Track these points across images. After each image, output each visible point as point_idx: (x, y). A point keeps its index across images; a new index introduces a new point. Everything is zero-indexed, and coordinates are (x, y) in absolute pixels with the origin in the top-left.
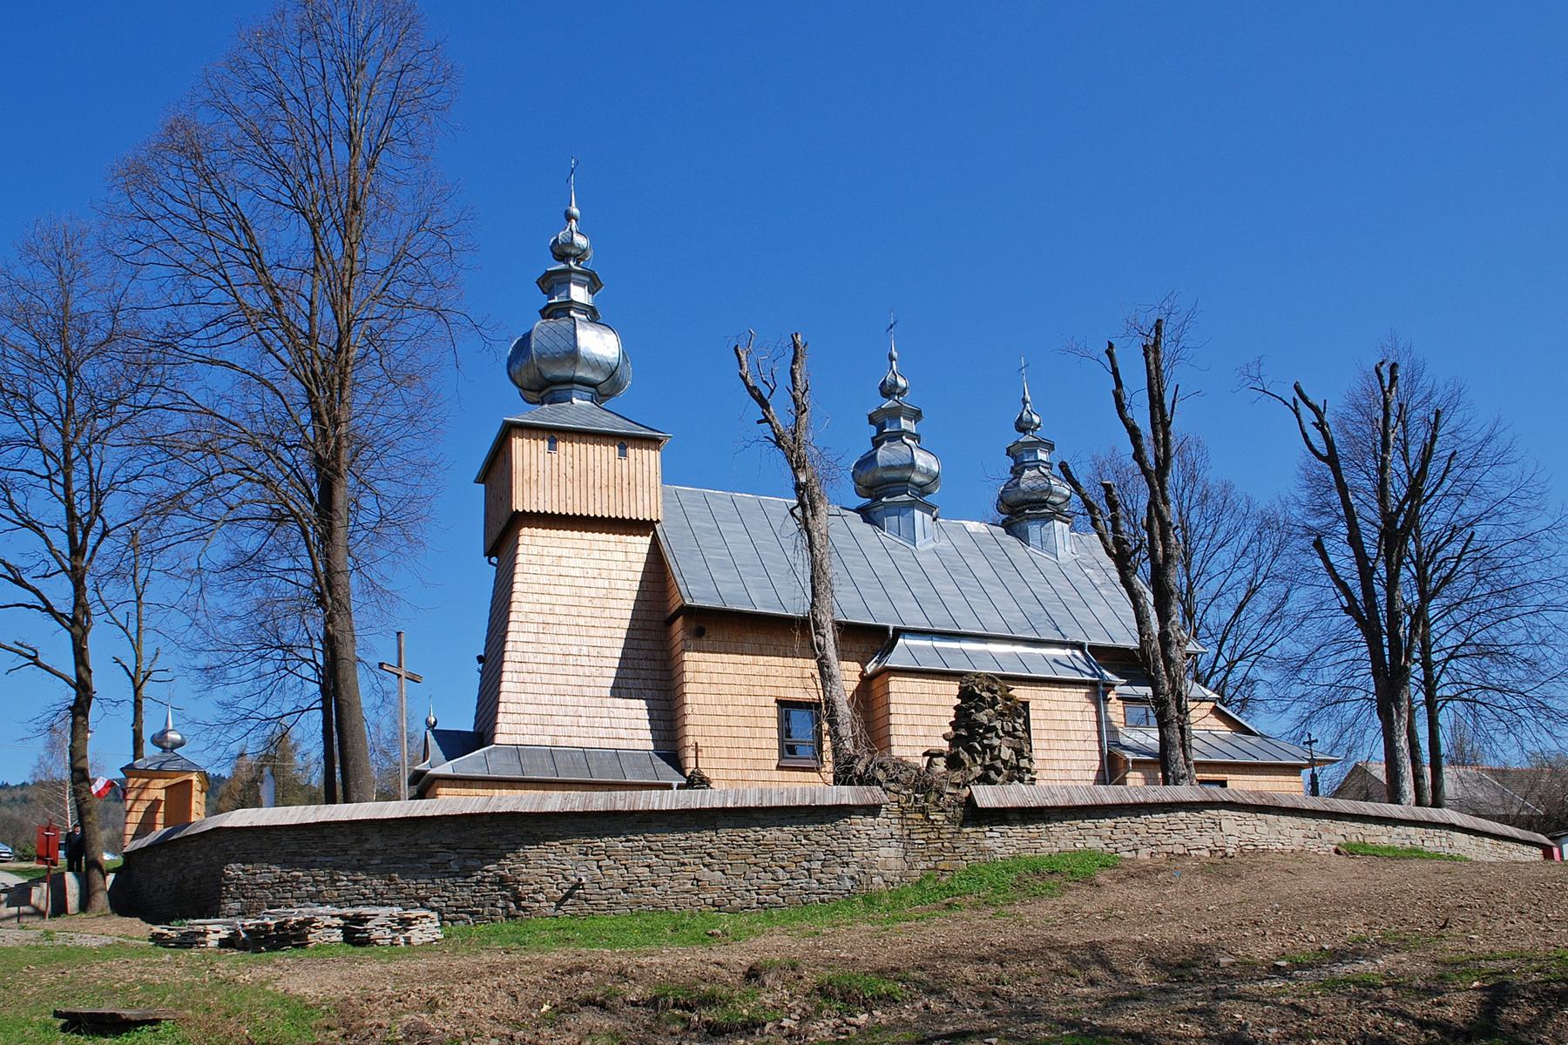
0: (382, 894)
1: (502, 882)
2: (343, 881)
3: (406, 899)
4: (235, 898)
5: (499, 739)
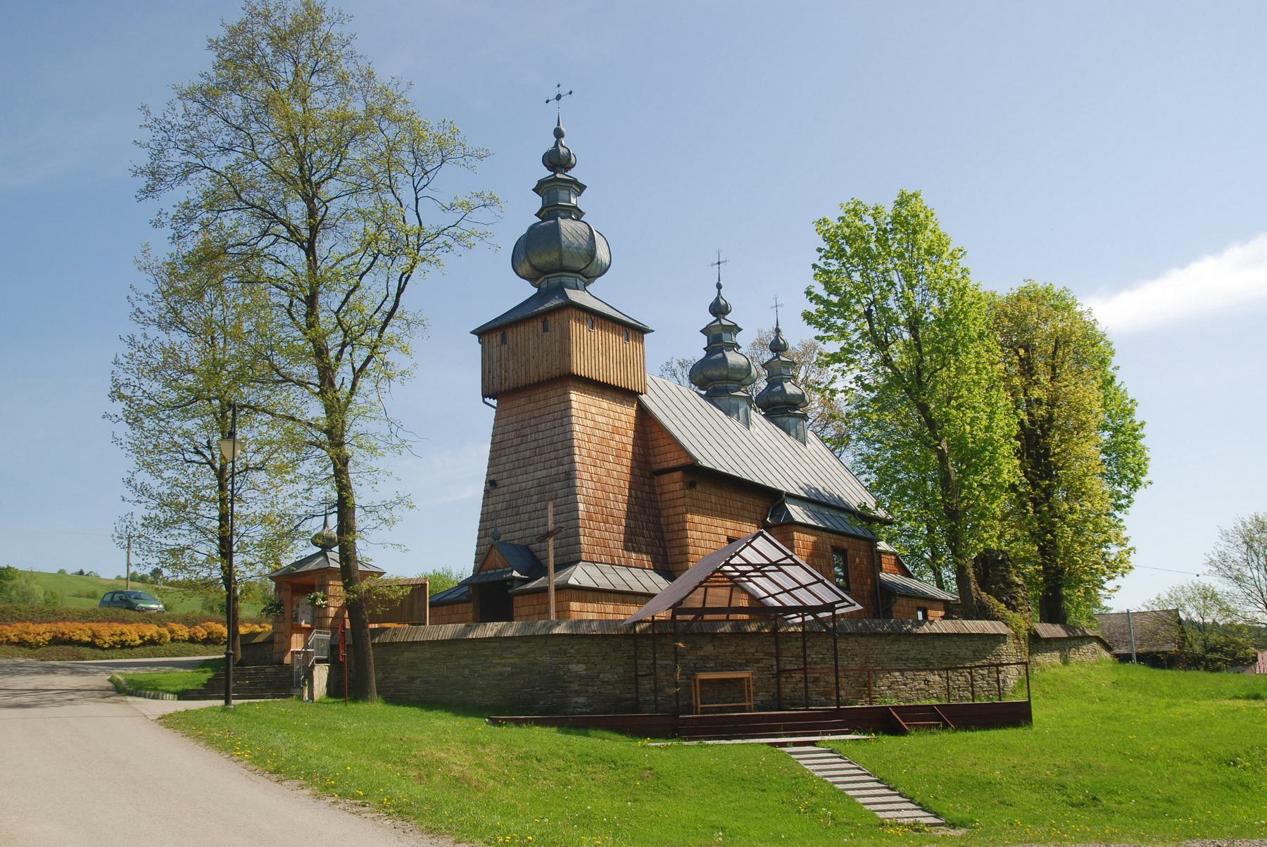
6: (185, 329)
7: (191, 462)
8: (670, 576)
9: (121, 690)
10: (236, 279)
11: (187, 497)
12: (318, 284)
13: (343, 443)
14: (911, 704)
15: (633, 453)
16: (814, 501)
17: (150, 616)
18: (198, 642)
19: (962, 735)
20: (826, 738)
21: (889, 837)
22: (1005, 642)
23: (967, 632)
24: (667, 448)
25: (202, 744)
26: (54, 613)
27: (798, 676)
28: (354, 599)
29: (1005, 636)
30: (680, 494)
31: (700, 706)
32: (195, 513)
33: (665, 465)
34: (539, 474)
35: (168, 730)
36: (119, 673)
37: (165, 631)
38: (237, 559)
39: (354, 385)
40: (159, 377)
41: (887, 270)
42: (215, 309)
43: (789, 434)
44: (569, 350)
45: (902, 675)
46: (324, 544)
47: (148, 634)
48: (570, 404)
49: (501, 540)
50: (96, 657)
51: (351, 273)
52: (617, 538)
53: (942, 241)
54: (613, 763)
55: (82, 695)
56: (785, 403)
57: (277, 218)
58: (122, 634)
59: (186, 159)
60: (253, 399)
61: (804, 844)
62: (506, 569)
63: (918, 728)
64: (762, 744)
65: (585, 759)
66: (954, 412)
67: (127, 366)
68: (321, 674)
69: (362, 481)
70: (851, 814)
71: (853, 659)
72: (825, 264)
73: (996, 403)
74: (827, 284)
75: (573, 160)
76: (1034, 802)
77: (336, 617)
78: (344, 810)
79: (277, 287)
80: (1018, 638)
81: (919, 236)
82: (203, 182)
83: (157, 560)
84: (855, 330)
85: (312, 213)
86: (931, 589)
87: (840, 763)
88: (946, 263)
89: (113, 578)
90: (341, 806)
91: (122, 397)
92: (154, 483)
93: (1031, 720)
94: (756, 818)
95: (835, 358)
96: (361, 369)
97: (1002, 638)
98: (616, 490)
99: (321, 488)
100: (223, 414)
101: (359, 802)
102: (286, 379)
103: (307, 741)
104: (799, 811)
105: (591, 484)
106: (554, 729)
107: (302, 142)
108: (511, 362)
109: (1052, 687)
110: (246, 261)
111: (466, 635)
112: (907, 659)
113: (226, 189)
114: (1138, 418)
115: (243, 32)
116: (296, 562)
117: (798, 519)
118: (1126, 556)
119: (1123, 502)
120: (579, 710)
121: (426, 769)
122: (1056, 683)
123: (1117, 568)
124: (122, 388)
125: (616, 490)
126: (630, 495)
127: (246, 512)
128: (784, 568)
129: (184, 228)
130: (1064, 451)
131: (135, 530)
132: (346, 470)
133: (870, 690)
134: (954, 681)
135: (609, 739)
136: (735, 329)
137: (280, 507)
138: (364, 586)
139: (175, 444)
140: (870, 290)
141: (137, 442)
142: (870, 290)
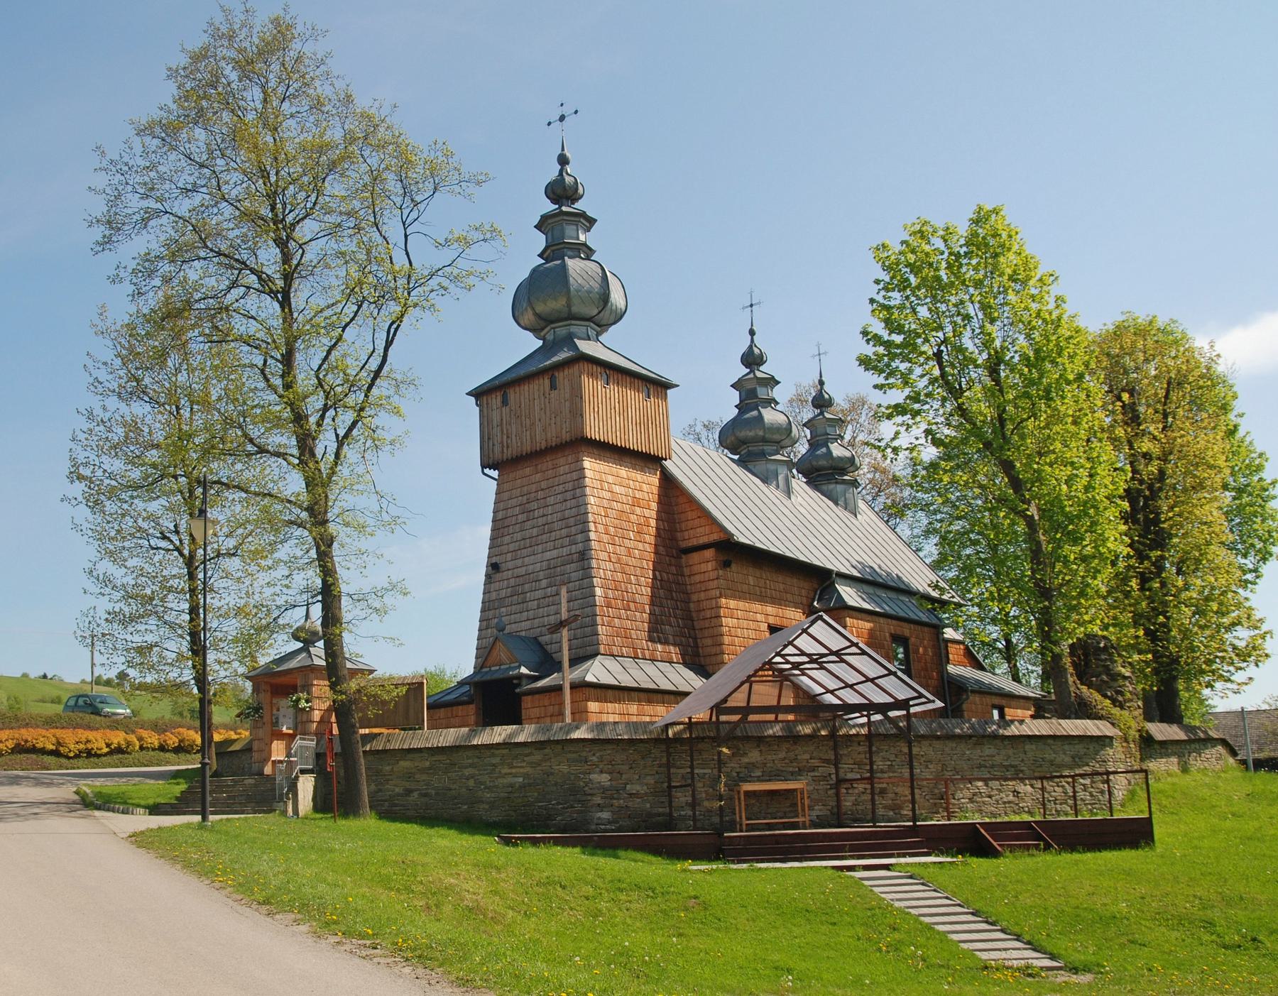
6: (147, 399)
7: (157, 548)
8: (704, 671)
9: (88, 803)
10: (201, 339)
11: (154, 587)
12: (296, 338)
13: (327, 521)
14: (998, 820)
15: (657, 529)
16: (868, 582)
17: (117, 722)
18: (168, 751)
19: (1067, 857)
20: (902, 860)
21: (996, 983)
22: (1111, 746)
23: (1065, 733)
24: (697, 522)
25: (179, 867)
26: (16, 718)
27: (860, 787)
28: (342, 701)
29: (1111, 738)
30: (713, 575)
31: (745, 822)
32: (162, 606)
33: (694, 542)
34: (548, 555)
35: (140, 850)
36: (85, 785)
37: (133, 738)
38: (211, 657)
39: (337, 455)
40: (120, 454)
41: (962, 302)
42: (179, 375)
43: (836, 504)
44: (582, 410)
45: (987, 785)
46: (306, 638)
47: (116, 741)
48: (584, 473)
49: (506, 632)
50: (61, 767)
51: (332, 325)
52: (641, 628)
53: (1027, 264)
54: (650, 891)
55: (48, 809)
56: (832, 468)
57: (246, 266)
58: (88, 741)
59: (145, 203)
60: (224, 475)
61: (893, 990)
62: (513, 665)
63: (1012, 849)
64: (826, 867)
65: (618, 885)
66: (1047, 468)
67: (85, 442)
68: (306, 786)
69: (349, 565)
70: (945, 954)
71: (927, 767)
72: (884, 297)
73: (1098, 457)
74: (888, 322)
75: (580, 190)
76: (1175, 942)
77: (321, 721)
78: (351, 952)
79: (249, 345)
80: (1126, 741)
81: (1002, 259)
82: (164, 228)
83: (123, 659)
84: (922, 376)
85: (286, 258)
86: (1009, 685)
87: (924, 891)
88: (1033, 291)
89: (78, 681)
90: (347, 947)
91: (81, 478)
92: (118, 573)
93: (1153, 840)
94: (828, 957)
95: (899, 409)
96: (346, 436)
97: (1108, 740)
98: (638, 572)
99: (302, 574)
100: (191, 492)
101: (368, 942)
102: (262, 450)
103: (297, 865)
104: (880, 950)
105: (609, 566)
106: (577, 850)
107: (273, 179)
108: (514, 426)
109: (1170, 799)
110: (213, 317)
111: (470, 741)
112: (992, 766)
113: (190, 237)
114: (1268, 475)
115: (205, 57)
116: (275, 660)
117: (851, 602)
118: (1260, 641)
119: (1249, 577)
120: (603, 827)
121: (435, 898)
122: (1176, 795)
123: (1250, 657)
124: (81, 468)
125: (638, 572)
126: (655, 578)
127: (219, 604)
128: (844, 657)
129: (144, 283)
130: (1180, 515)
131: (98, 626)
132: (331, 552)
133: (948, 803)
134: (1049, 793)
135: (642, 861)
136: (772, 382)
137: (256, 597)
138: (353, 685)
139: (140, 529)
140: (940, 328)
141: (98, 528)
142: (940, 328)
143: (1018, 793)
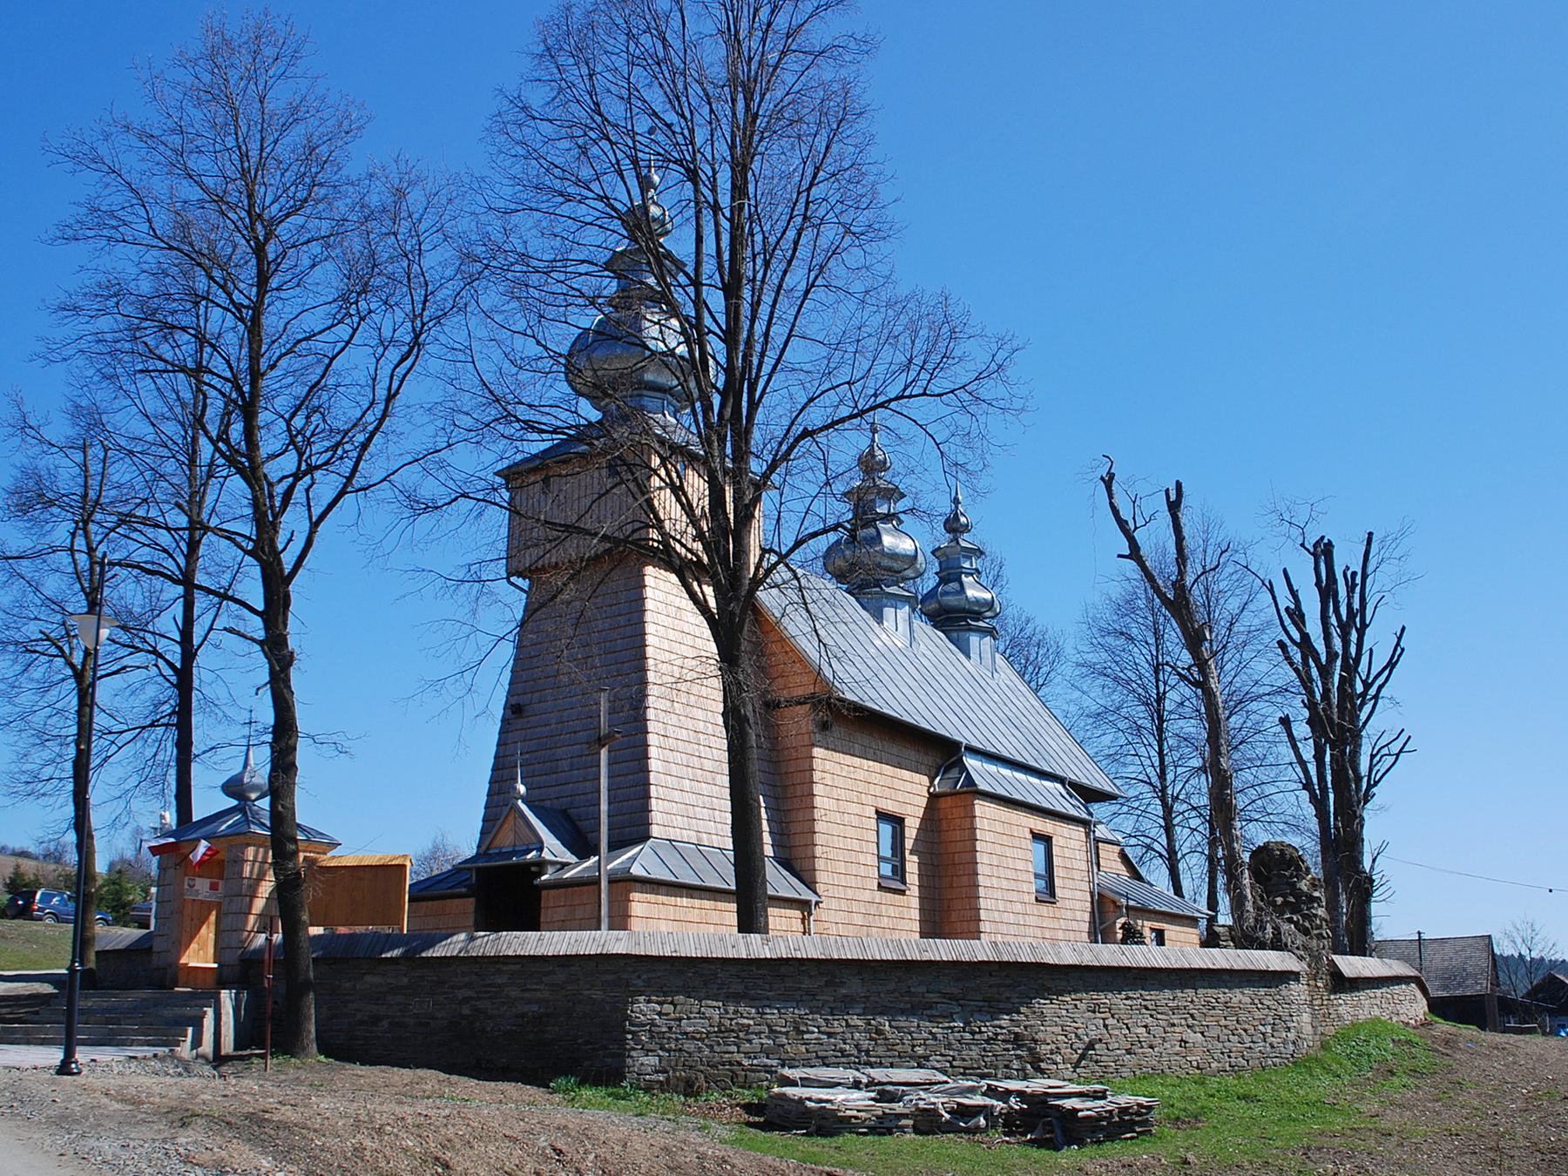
0: (867, 1052)
1: (1017, 1040)
2: (813, 1032)
3: (900, 1057)
4: (648, 1051)
5: (655, 831)
143: (1186, 1042)
